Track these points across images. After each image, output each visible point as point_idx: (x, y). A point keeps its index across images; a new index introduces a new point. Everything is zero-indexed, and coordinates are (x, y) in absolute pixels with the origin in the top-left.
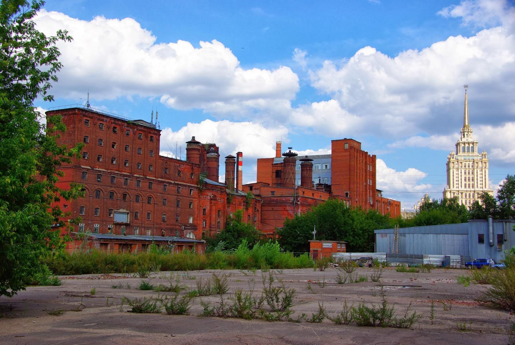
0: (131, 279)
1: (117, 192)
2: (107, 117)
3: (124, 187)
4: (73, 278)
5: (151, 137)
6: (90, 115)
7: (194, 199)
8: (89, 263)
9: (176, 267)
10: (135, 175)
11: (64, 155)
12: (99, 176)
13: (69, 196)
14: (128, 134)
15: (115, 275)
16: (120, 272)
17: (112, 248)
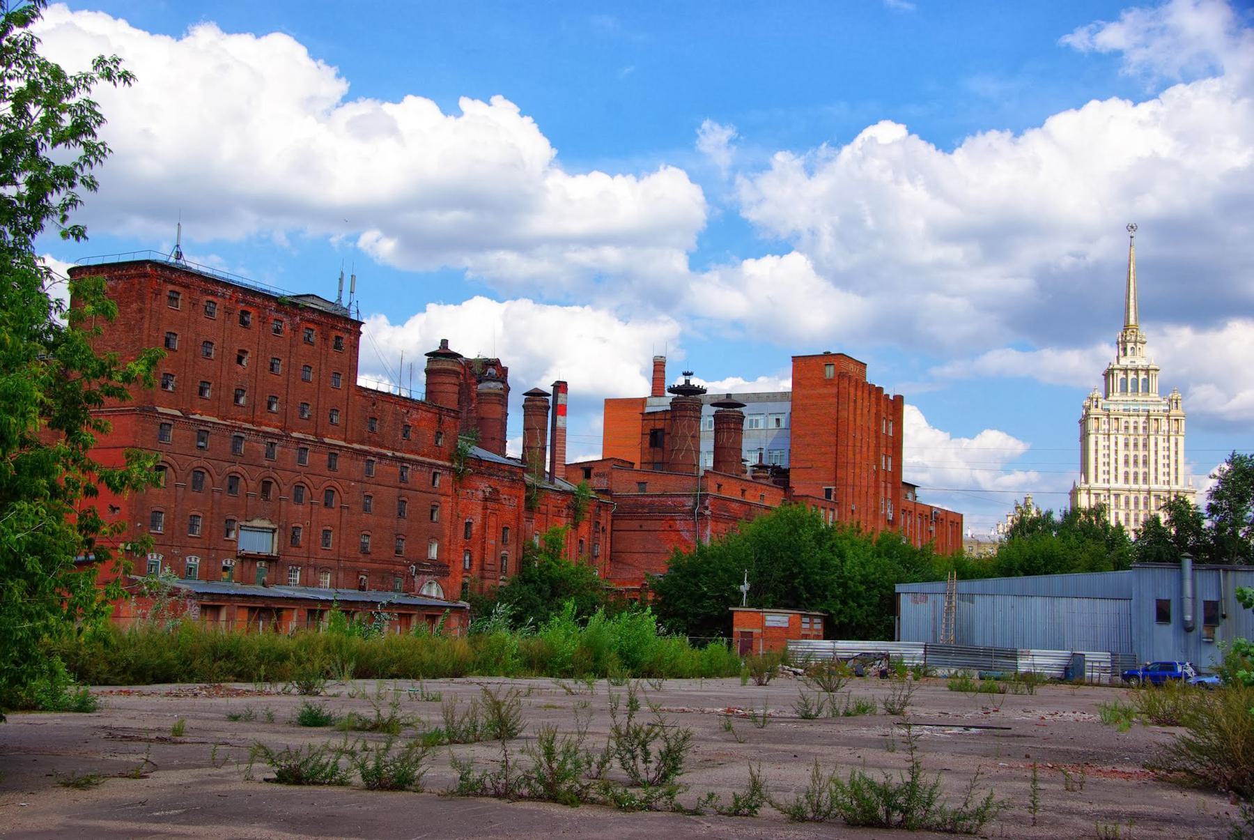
0: (278, 698)
1: (246, 475)
2: (227, 285)
3: (266, 463)
4: (129, 693)
5: (338, 338)
6: (184, 279)
7: (443, 499)
8: (171, 654)
9: (394, 669)
10: (295, 435)
11: (110, 378)
12: (202, 435)
13: (123, 484)
14: (277, 331)
15: (237, 686)
16: (249, 679)
17: (230, 618)
